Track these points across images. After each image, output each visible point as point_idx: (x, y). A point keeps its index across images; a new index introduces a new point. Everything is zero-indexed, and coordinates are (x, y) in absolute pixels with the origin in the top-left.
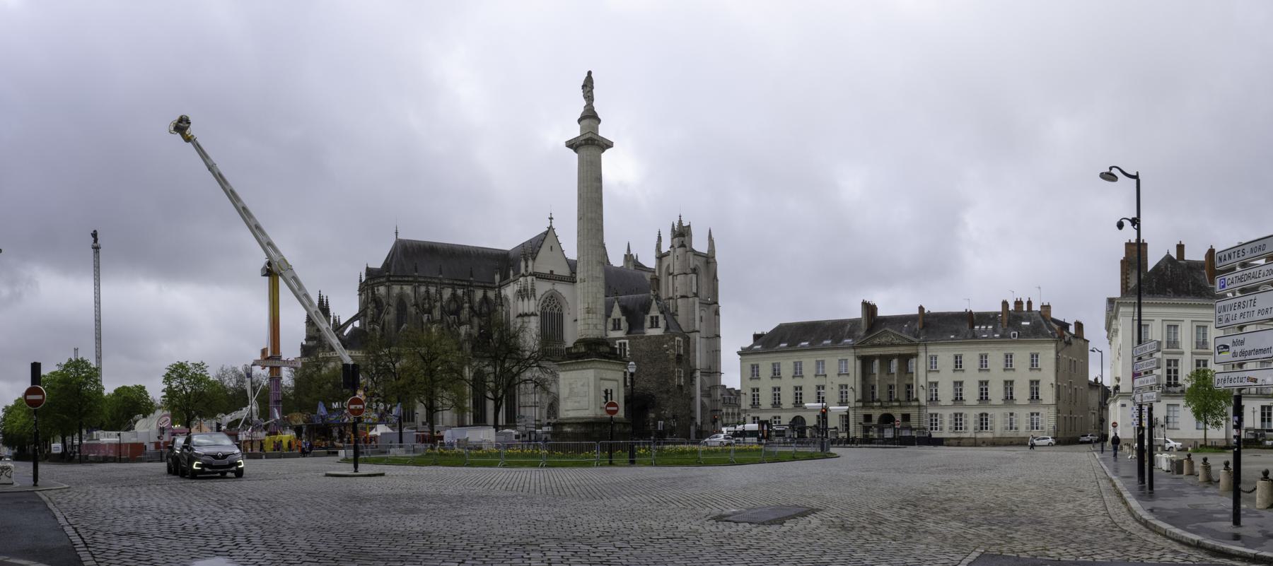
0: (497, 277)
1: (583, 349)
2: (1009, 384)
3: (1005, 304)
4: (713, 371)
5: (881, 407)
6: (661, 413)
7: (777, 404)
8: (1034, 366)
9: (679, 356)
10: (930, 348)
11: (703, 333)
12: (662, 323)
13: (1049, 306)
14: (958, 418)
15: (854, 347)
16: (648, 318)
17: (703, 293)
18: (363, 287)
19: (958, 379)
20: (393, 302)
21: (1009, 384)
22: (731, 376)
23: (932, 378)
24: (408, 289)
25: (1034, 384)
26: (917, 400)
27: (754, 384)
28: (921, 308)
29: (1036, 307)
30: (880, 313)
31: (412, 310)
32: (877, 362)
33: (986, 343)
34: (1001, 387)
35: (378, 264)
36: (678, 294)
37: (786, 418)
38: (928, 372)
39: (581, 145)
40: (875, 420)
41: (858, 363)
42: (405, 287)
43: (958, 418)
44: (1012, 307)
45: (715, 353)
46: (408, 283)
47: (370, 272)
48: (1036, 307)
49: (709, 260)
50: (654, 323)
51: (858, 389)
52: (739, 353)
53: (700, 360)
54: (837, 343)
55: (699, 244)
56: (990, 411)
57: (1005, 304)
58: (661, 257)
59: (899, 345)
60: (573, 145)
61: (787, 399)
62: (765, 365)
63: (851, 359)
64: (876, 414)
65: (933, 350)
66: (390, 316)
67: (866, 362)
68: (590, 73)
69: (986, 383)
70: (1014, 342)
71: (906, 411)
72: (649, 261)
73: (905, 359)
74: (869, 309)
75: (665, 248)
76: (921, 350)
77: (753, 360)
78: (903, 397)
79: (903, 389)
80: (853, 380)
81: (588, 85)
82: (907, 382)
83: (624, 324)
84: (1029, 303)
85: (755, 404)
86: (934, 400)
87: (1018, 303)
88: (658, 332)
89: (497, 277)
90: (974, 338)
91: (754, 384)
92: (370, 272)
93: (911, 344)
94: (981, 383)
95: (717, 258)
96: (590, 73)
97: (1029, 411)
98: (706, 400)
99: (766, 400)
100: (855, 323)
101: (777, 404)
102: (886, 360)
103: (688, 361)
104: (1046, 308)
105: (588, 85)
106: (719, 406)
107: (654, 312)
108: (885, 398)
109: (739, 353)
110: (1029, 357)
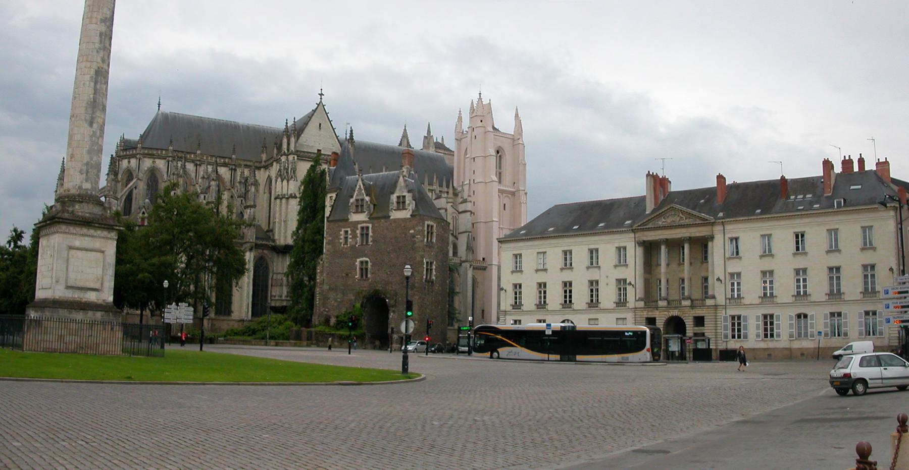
2: (594, 285)
3: (827, 165)
8: (868, 246)
10: (728, 227)
13: (886, 163)
14: (768, 321)
15: (634, 231)
16: (394, 198)
19: (801, 266)
21: (594, 285)
23: (733, 267)
24: (161, 164)
25: (869, 269)
26: (714, 297)
29: (870, 166)
30: (674, 187)
33: (802, 216)
34: (824, 276)
38: (726, 260)
41: (640, 251)
42: (157, 161)
43: (768, 321)
44: (838, 169)
46: (160, 157)
48: (870, 166)
50: (401, 203)
51: (640, 284)
54: (614, 227)
56: (843, 309)
57: (827, 165)
63: (631, 246)
65: (735, 229)
67: (650, 249)
69: (805, 271)
71: (699, 312)
73: (702, 245)
76: (718, 229)
78: (697, 294)
79: (698, 283)
80: (633, 271)
82: (704, 274)
84: (861, 161)
86: (736, 299)
87: (847, 163)
88: (405, 214)
90: (790, 211)
93: (706, 223)
94: (591, 283)
97: (862, 309)
102: (675, 245)
104: (883, 166)
110: (859, 231)
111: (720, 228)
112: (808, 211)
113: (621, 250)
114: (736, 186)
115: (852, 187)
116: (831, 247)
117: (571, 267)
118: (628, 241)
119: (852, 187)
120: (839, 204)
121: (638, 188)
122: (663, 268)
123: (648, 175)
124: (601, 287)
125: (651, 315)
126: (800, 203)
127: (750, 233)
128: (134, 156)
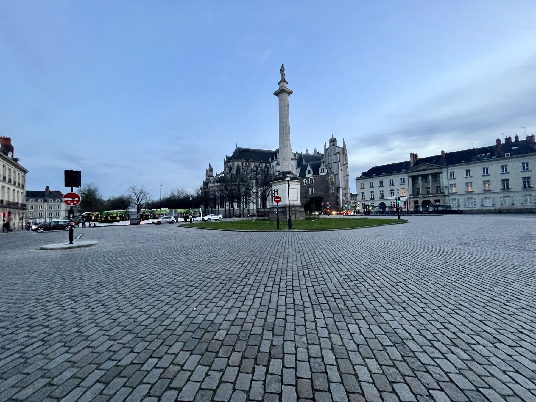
0: (270, 159)
1: (281, 176)
3: (498, 141)
4: (346, 188)
5: (423, 197)
6: (320, 201)
7: (372, 198)
9: (332, 182)
10: (449, 168)
11: (342, 175)
12: (326, 171)
15: (407, 173)
16: (320, 169)
17: (342, 161)
18: (226, 163)
20: (235, 168)
22: (353, 189)
24: (240, 163)
26: (443, 193)
27: (363, 191)
28: (443, 152)
29: (503, 141)
30: (419, 157)
31: (241, 170)
32: (420, 178)
35: (230, 155)
36: (333, 162)
37: (377, 204)
39: (279, 93)
40: (420, 202)
41: (410, 179)
45: (347, 181)
46: (240, 161)
47: (227, 158)
48: (503, 141)
49: (344, 149)
50: (323, 171)
52: (356, 180)
53: (341, 185)
55: (340, 144)
58: (326, 150)
59: (431, 169)
60: (277, 94)
61: (377, 196)
62: (367, 182)
64: (420, 201)
66: (235, 172)
67: (414, 179)
68: (283, 65)
70: (507, 158)
72: (322, 152)
74: (414, 156)
75: (328, 146)
76: (444, 170)
77: (361, 181)
81: (282, 70)
83: (312, 172)
85: (363, 199)
89: (270, 159)
90: (479, 160)
91: (363, 191)
92: (227, 158)
95: (346, 148)
96: (283, 65)
98: (344, 198)
99: (368, 197)
100: (408, 163)
101: (372, 198)
102: (425, 177)
103: (336, 184)
105: (282, 70)
106: (349, 200)
107: (322, 167)
108: (425, 193)
109: (356, 180)
111: (446, 169)
112: (490, 159)
113: (403, 180)
114: (447, 154)
115: (513, 148)
116: (503, 171)
117: (364, 188)
118: (405, 176)
119: (513, 148)
120: (508, 155)
121: (408, 158)
122: (420, 184)
123: (411, 154)
124: (384, 193)
125: (416, 200)
126: (484, 157)
127: (459, 171)
128: (231, 162)
